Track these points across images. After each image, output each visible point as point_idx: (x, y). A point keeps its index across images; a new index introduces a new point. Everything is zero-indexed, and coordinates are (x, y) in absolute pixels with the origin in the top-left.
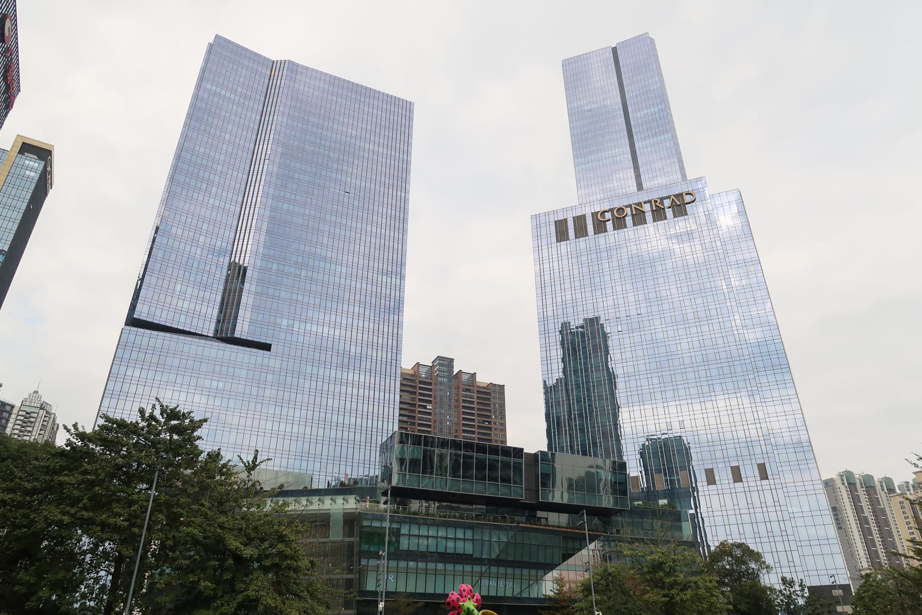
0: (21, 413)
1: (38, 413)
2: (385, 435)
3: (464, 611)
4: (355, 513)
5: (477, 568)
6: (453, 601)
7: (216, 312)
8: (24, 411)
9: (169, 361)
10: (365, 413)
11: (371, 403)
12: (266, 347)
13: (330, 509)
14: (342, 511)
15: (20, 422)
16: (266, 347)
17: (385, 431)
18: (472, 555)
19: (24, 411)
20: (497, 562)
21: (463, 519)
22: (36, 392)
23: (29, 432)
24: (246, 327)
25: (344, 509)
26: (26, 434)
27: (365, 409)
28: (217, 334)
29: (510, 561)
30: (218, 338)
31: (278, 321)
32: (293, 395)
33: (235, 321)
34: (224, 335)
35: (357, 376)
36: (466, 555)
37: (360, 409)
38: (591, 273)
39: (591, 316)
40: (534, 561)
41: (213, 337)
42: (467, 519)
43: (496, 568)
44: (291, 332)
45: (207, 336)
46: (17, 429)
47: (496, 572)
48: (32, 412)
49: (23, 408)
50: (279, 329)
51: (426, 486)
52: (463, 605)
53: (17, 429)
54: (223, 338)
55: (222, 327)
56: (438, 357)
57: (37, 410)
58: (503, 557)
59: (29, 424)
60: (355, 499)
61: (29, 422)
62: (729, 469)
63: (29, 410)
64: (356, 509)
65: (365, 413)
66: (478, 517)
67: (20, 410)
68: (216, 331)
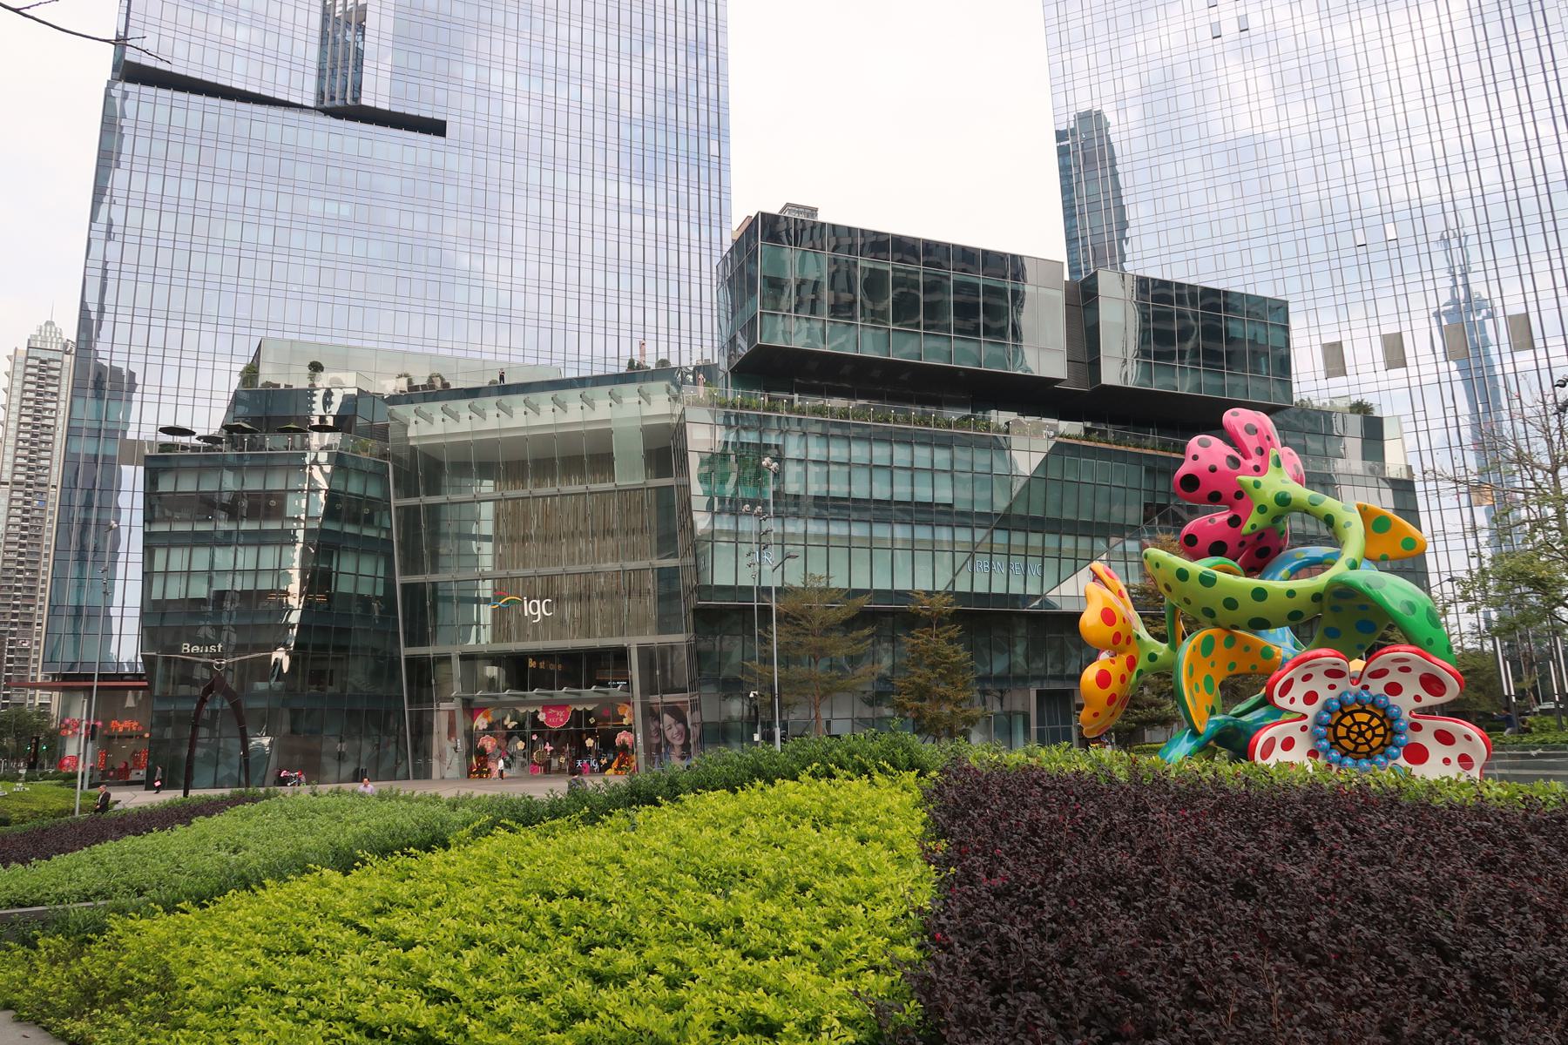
0: (30, 362)
1: (62, 361)
2: (716, 253)
3: (1262, 509)
4: (668, 425)
5: (963, 535)
6: (1213, 470)
7: (314, 52)
8: (36, 358)
9: (223, 159)
10: (662, 269)
11: (673, 247)
12: (436, 128)
13: (608, 421)
14: (639, 424)
15: (32, 379)
16: (436, 128)
17: (716, 246)
18: (950, 506)
19: (36, 358)
20: (1005, 521)
21: (927, 424)
22: (50, 323)
23: (54, 394)
24: (384, 85)
25: (644, 418)
26: (48, 398)
27: (662, 260)
28: (322, 102)
29: (1035, 519)
30: (321, 110)
31: (456, 69)
32: (507, 231)
33: (358, 78)
34: (338, 103)
35: (637, 191)
36: (938, 505)
37: (650, 258)
38: (1087, 13)
39: (1084, 107)
40: (1084, 518)
41: (315, 109)
42: (938, 426)
43: (1006, 533)
44: (487, 94)
45: (301, 107)
46: (31, 391)
47: (1006, 542)
48: (50, 360)
49: (32, 353)
50: (459, 88)
51: (842, 346)
52: (1257, 485)
53: (31, 391)
54: (337, 108)
55: (331, 86)
56: (788, 205)
57: (58, 356)
58: (1020, 510)
59: (50, 381)
60: (668, 391)
61: (49, 376)
62: (1410, 361)
63: (45, 356)
64: (672, 415)
65: (662, 269)
66: (958, 424)
67: (28, 358)
68: (321, 94)
